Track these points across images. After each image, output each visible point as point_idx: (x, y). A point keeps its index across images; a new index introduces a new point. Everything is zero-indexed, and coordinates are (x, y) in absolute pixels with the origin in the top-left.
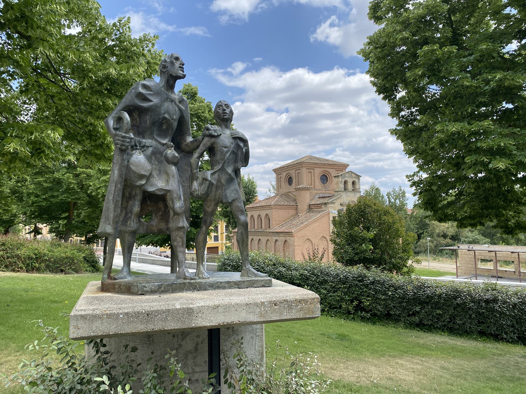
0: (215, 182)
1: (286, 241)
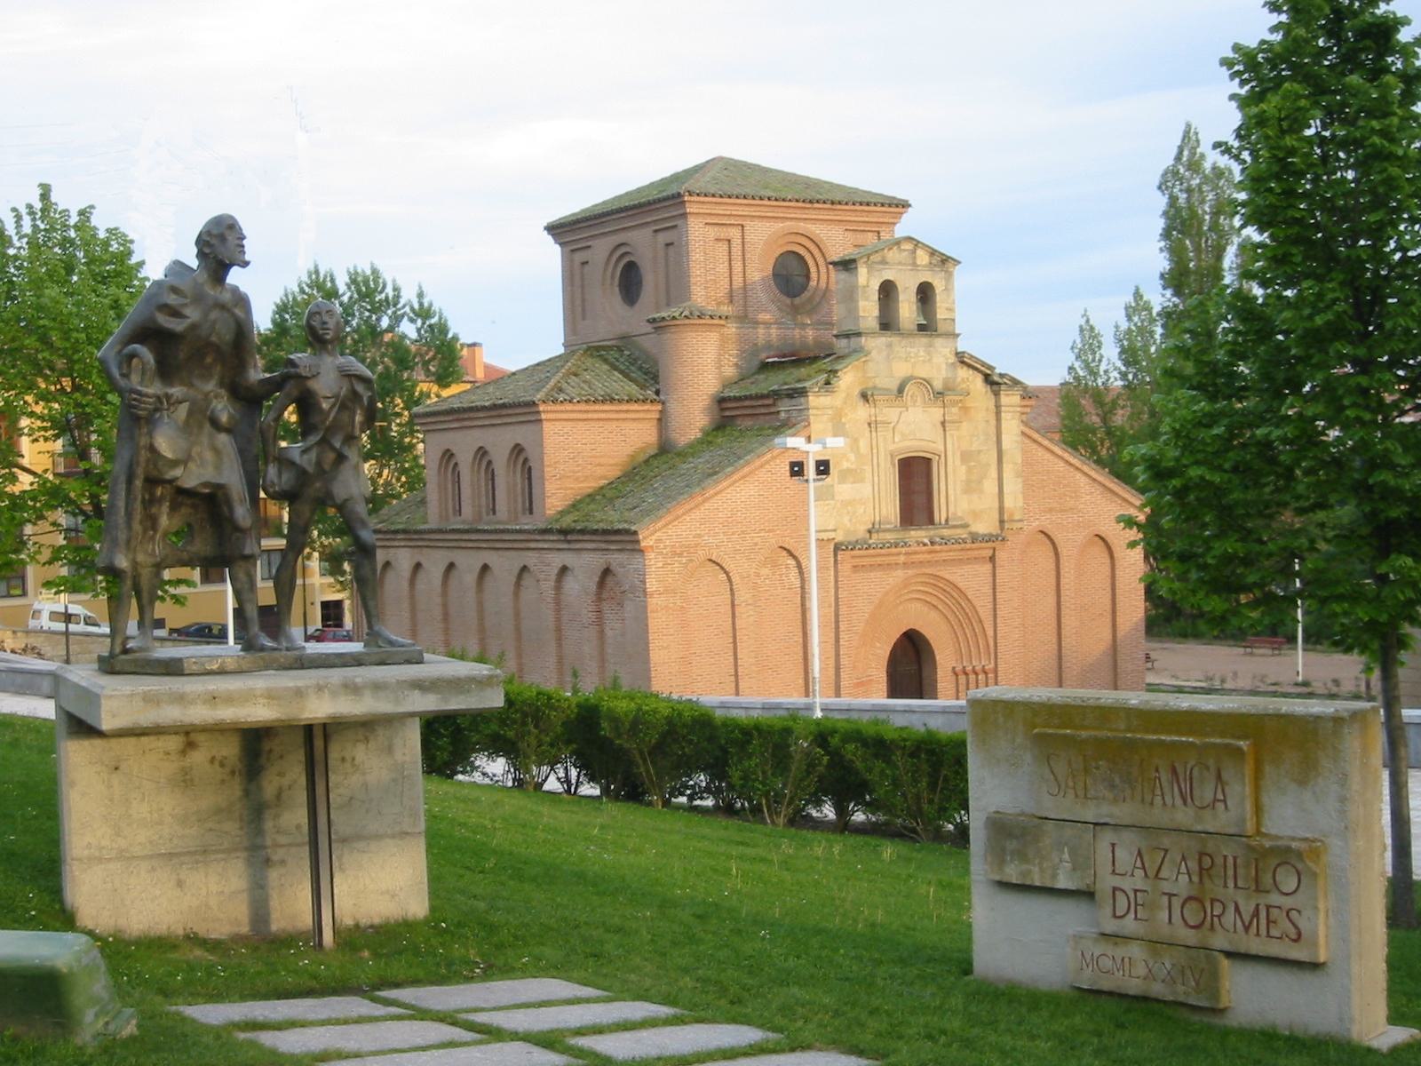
1: (607, 572)
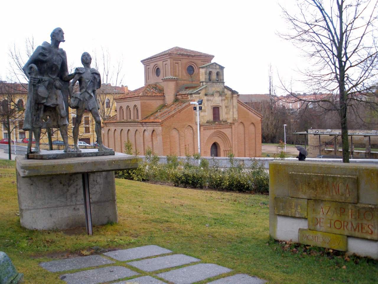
0: (82, 99)
1: (154, 131)
